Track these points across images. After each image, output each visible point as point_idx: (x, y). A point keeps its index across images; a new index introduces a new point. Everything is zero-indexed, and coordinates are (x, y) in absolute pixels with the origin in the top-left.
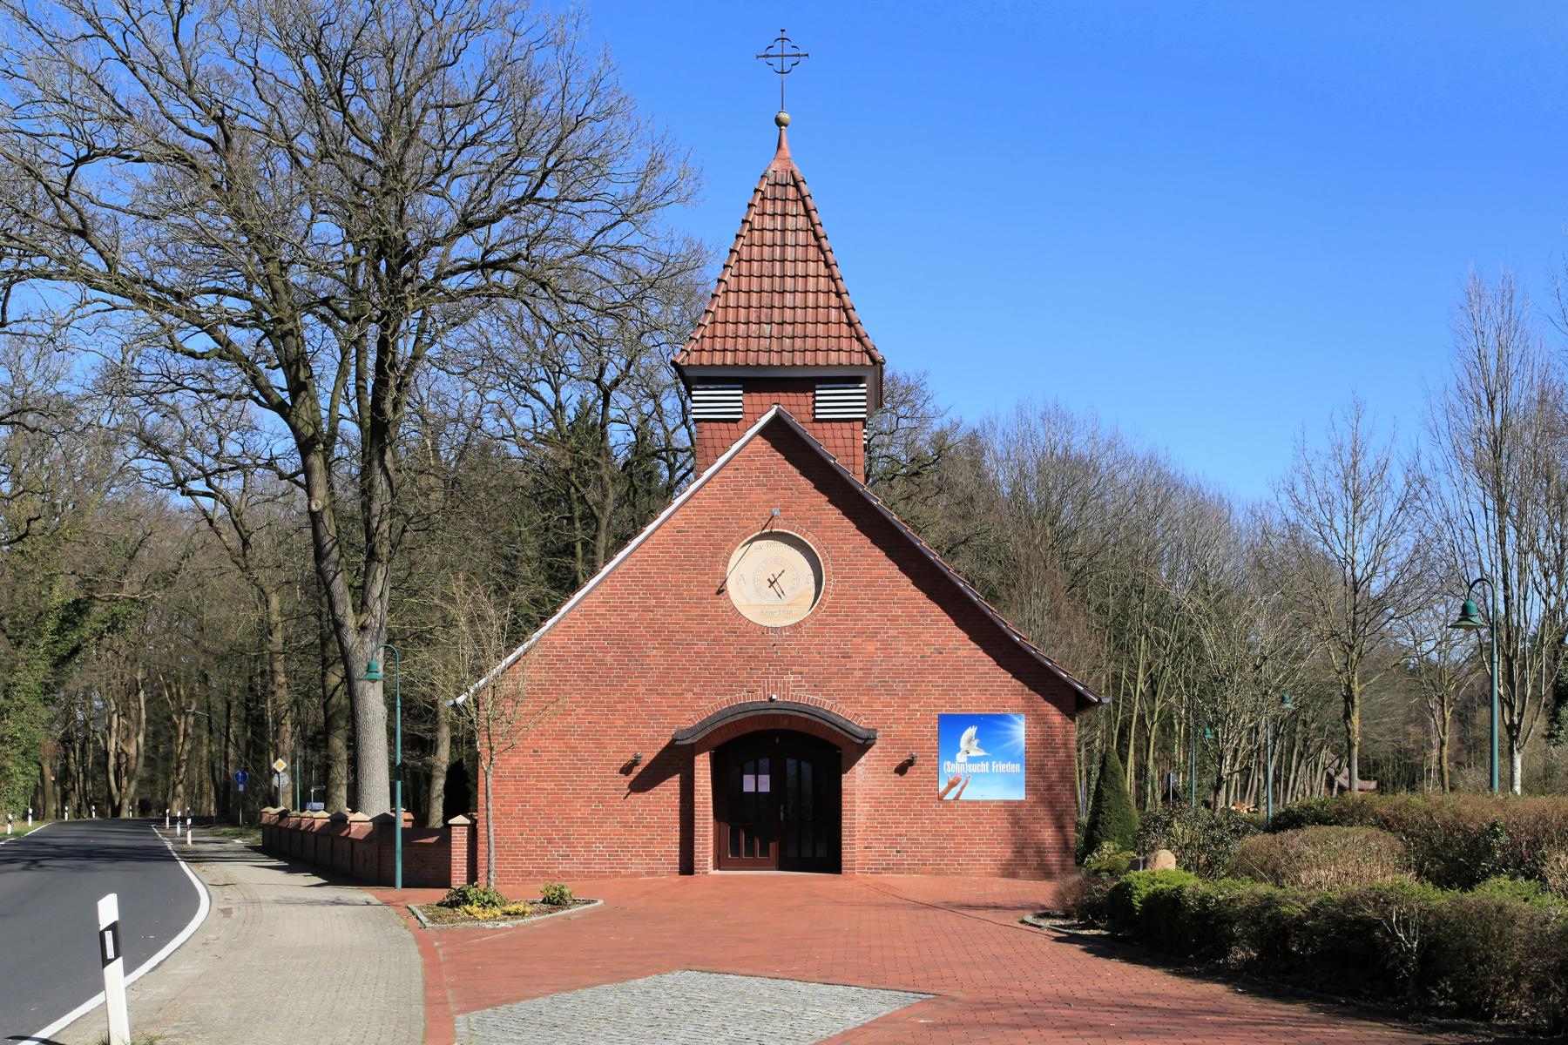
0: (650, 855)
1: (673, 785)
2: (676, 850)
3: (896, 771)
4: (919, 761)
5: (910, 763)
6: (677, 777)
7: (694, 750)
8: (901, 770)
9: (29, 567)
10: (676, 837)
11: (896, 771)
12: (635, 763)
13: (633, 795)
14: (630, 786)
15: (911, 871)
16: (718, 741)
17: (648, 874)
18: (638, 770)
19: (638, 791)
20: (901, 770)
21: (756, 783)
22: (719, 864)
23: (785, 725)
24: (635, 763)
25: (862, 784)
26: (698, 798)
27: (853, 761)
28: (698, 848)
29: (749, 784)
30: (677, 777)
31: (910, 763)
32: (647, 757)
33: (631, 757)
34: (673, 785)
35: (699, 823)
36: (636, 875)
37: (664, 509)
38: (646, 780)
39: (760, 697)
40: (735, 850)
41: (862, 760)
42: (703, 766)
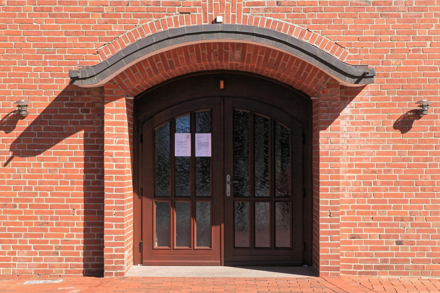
0: (42, 247)
1: (74, 146)
2: (78, 241)
3: (397, 126)
4: (430, 112)
5: (418, 114)
6: (80, 136)
7: (103, 95)
8: (404, 125)
9: (165, 208)
10: (79, 222)
11: (397, 126)
12: (18, 115)
13: (17, 160)
14: (12, 148)
15: (418, 270)
16: (142, 83)
17: (39, 274)
18: (23, 125)
19: (25, 154)
20: (404, 125)
21: (191, 144)
22: (142, 256)
23: (234, 62)
24: (18, 115)
25: (346, 144)
26: (109, 165)
27: (335, 113)
28: (109, 239)
29: (182, 147)
30: (80, 136)
31: (418, 114)
32: (36, 108)
33: (13, 107)
34: (74, 146)
35: (110, 202)
36: (21, 276)
37: (77, 14)
38: (36, 140)
39: (198, 20)
40: (165, 239)
41: (347, 111)
42: (117, 118)
